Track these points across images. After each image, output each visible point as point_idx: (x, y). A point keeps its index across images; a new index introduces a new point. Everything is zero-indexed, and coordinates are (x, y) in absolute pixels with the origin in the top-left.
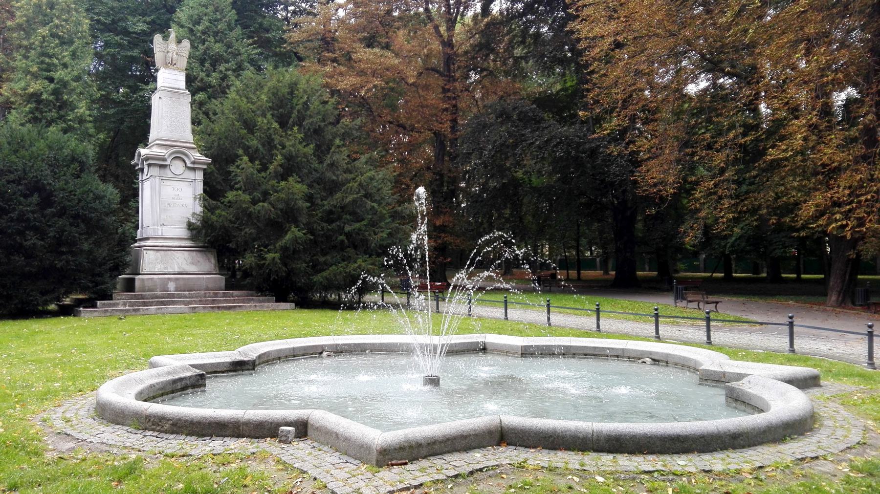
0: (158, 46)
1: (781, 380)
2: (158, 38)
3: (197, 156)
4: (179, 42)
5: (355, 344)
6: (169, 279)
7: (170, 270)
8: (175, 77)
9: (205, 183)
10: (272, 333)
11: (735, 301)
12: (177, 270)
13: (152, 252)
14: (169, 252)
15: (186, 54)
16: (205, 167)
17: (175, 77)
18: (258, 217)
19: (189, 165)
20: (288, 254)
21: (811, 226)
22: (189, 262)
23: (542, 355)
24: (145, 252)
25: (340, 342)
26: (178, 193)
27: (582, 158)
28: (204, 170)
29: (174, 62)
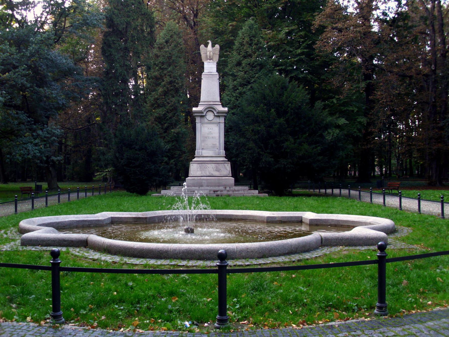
2: (202, 46)
3: (221, 108)
7: (205, 174)
8: (210, 66)
10: (277, 206)
12: (208, 174)
15: (217, 52)
16: (225, 115)
17: (210, 66)
18: (126, 47)
19: (216, 114)
21: (431, 172)
26: (211, 130)
27: (282, 294)
28: (225, 116)
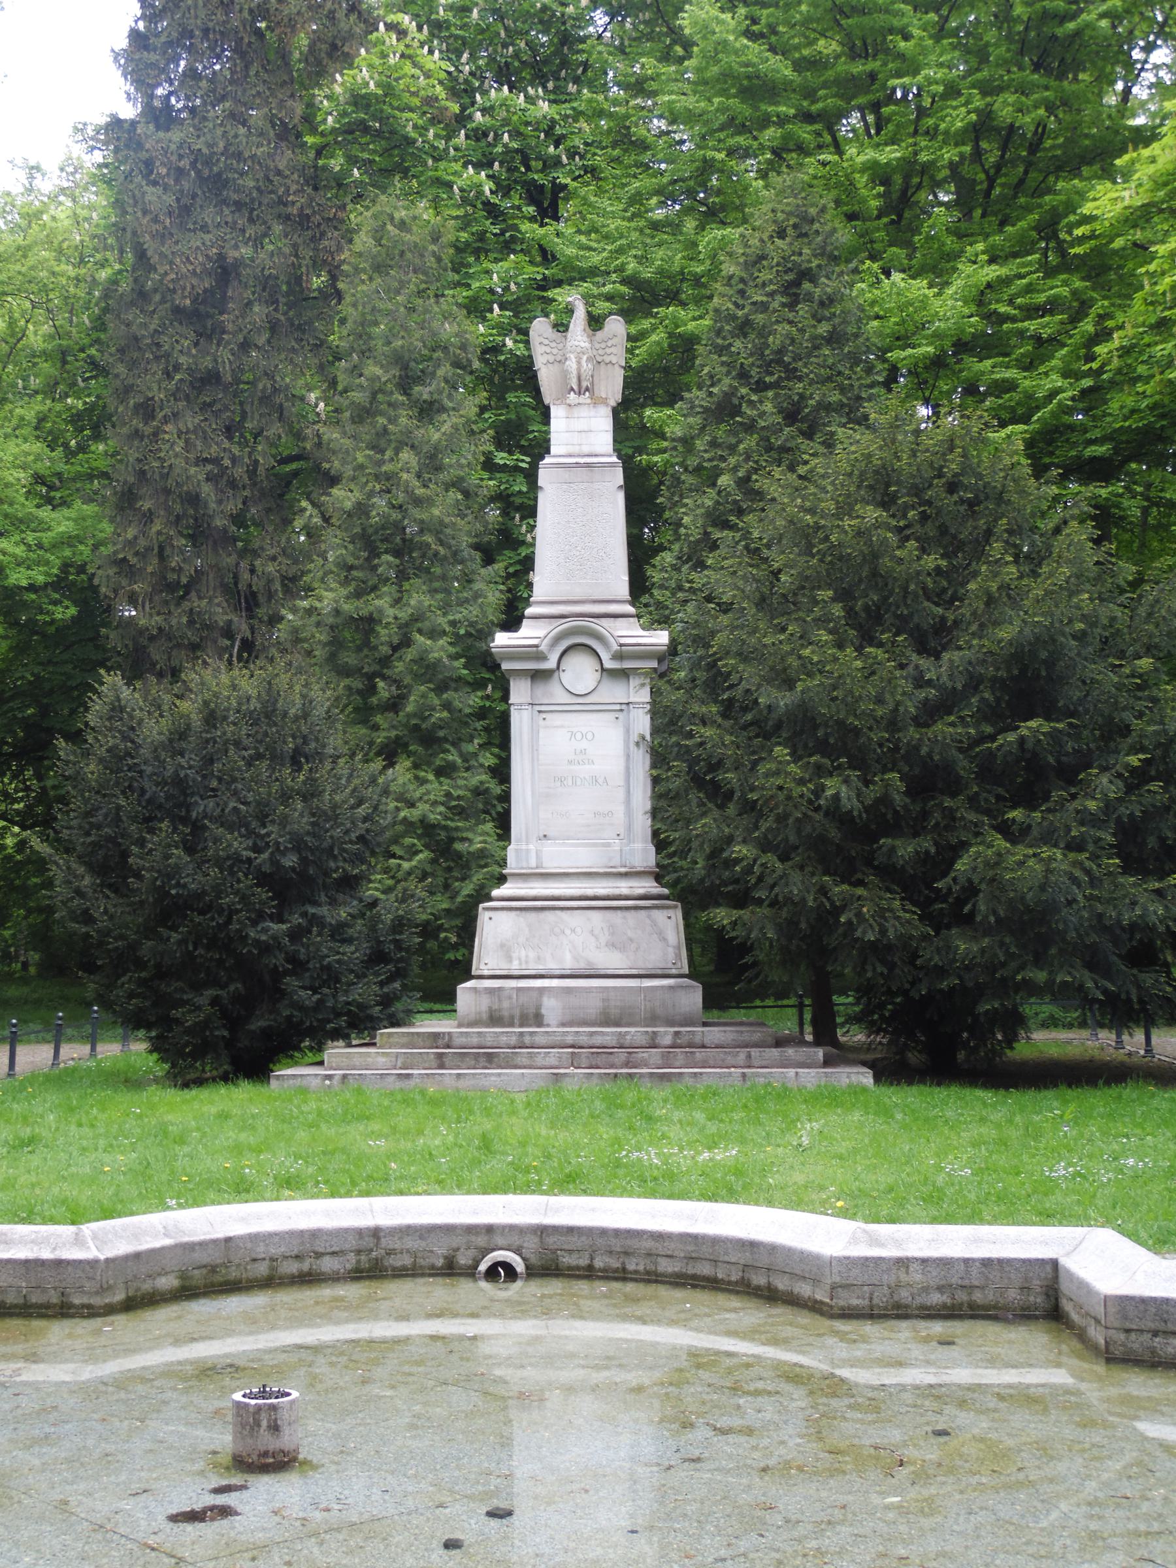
0: (544, 349)
1: (1070, 1325)
4: (595, 322)
5: (987, 1263)
6: (542, 990)
7: (552, 966)
9: (656, 711)
11: (605, 1296)
12: (568, 963)
13: (503, 914)
14: (549, 916)
15: (617, 355)
16: (655, 664)
19: (609, 664)
20: (963, 818)
22: (603, 939)
23: (187, 1292)
24: (487, 914)
25: (133, 1366)
26: (584, 744)
29: (585, 384)
